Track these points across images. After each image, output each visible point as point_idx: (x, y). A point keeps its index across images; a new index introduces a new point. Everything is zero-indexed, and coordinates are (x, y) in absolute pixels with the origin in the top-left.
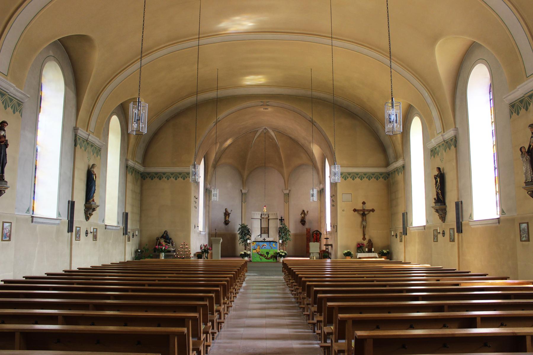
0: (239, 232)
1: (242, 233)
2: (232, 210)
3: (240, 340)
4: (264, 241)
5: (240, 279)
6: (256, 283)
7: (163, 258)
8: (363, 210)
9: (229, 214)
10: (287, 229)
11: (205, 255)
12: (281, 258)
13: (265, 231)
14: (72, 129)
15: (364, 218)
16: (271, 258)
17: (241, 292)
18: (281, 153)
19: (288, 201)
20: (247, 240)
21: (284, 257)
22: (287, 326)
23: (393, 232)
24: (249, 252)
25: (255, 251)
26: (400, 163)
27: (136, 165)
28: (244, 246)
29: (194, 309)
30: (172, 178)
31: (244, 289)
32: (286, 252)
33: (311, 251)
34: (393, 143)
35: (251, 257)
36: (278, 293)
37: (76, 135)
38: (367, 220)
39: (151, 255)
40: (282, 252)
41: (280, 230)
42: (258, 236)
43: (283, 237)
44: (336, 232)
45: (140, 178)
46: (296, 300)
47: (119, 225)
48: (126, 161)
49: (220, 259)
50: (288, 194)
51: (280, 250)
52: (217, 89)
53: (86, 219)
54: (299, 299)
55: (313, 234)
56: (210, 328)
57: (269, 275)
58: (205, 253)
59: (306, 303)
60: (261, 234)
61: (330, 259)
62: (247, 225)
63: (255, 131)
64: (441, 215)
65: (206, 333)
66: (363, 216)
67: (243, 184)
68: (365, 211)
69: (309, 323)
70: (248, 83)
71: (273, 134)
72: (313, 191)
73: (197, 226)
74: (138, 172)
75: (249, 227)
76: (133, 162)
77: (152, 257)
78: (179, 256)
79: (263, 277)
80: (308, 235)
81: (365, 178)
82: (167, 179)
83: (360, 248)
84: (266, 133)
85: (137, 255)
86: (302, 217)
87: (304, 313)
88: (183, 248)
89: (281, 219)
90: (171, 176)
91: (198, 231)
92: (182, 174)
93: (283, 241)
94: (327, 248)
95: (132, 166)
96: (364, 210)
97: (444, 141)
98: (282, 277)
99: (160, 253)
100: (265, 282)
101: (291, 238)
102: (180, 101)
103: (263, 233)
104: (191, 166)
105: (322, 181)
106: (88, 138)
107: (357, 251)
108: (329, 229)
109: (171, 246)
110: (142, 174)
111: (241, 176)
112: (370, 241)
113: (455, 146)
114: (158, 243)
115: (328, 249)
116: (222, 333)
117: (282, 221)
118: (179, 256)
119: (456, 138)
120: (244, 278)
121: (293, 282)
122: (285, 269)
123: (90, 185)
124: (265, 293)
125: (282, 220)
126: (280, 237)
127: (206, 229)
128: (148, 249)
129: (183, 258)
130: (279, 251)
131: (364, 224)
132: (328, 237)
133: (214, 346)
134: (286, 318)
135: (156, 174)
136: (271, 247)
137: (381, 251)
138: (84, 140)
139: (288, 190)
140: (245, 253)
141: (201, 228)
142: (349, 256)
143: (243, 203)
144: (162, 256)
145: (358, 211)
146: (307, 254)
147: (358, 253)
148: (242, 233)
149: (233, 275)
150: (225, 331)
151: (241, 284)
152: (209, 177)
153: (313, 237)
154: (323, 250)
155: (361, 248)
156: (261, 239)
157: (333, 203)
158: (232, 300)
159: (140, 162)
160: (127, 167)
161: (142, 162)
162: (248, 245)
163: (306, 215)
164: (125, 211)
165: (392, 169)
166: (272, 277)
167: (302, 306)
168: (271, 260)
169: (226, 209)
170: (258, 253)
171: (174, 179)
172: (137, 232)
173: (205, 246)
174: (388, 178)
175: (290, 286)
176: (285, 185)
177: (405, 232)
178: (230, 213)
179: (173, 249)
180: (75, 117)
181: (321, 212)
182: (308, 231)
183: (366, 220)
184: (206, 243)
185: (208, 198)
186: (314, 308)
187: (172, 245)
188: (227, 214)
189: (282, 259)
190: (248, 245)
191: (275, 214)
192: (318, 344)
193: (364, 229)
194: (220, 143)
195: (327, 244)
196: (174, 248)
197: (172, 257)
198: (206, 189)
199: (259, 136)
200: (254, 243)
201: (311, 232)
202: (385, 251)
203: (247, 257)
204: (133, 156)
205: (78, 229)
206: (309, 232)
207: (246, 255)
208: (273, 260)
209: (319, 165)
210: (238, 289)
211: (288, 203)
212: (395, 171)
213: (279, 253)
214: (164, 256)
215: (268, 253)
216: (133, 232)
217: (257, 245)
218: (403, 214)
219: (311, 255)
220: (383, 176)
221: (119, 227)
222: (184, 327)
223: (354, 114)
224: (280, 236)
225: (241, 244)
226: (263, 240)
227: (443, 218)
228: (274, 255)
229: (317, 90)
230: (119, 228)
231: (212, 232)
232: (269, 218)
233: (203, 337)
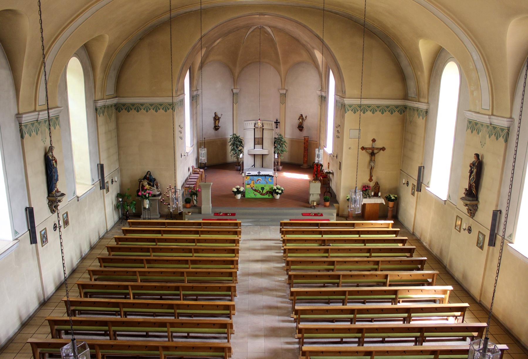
2: (222, 115)
8: (372, 149)
9: (219, 119)
12: (277, 195)
13: (259, 141)
14: (13, 117)
15: (373, 157)
16: (266, 194)
19: (285, 103)
23: (404, 180)
25: (249, 186)
30: (152, 110)
37: (20, 124)
38: (375, 160)
48: (95, 103)
50: (285, 95)
53: (52, 213)
64: (471, 210)
66: (372, 156)
71: (269, 30)
80: (306, 144)
82: (146, 111)
83: (365, 190)
89: (276, 121)
92: (163, 104)
96: (373, 149)
97: (491, 124)
106: (38, 118)
110: (116, 105)
111: (232, 72)
112: (377, 184)
113: (506, 141)
114: (141, 186)
117: (277, 125)
119: (509, 130)
123: (50, 174)
130: (275, 188)
131: (372, 165)
135: (133, 105)
143: (234, 104)
152: (195, 82)
160: (96, 110)
164: (100, 161)
168: (266, 196)
169: (215, 113)
170: (252, 188)
171: (154, 111)
172: (116, 178)
174: (405, 112)
178: (220, 118)
180: (16, 100)
183: (374, 161)
187: (157, 188)
188: (216, 119)
193: (372, 170)
200: (248, 177)
205: (43, 232)
208: (269, 196)
213: (275, 190)
214: (148, 203)
215: (263, 189)
216: (112, 178)
217: (251, 179)
218: (420, 168)
220: (398, 109)
224: (275, 147)
226: (258, 174)
227: (473, 210)
232: (263, 128)
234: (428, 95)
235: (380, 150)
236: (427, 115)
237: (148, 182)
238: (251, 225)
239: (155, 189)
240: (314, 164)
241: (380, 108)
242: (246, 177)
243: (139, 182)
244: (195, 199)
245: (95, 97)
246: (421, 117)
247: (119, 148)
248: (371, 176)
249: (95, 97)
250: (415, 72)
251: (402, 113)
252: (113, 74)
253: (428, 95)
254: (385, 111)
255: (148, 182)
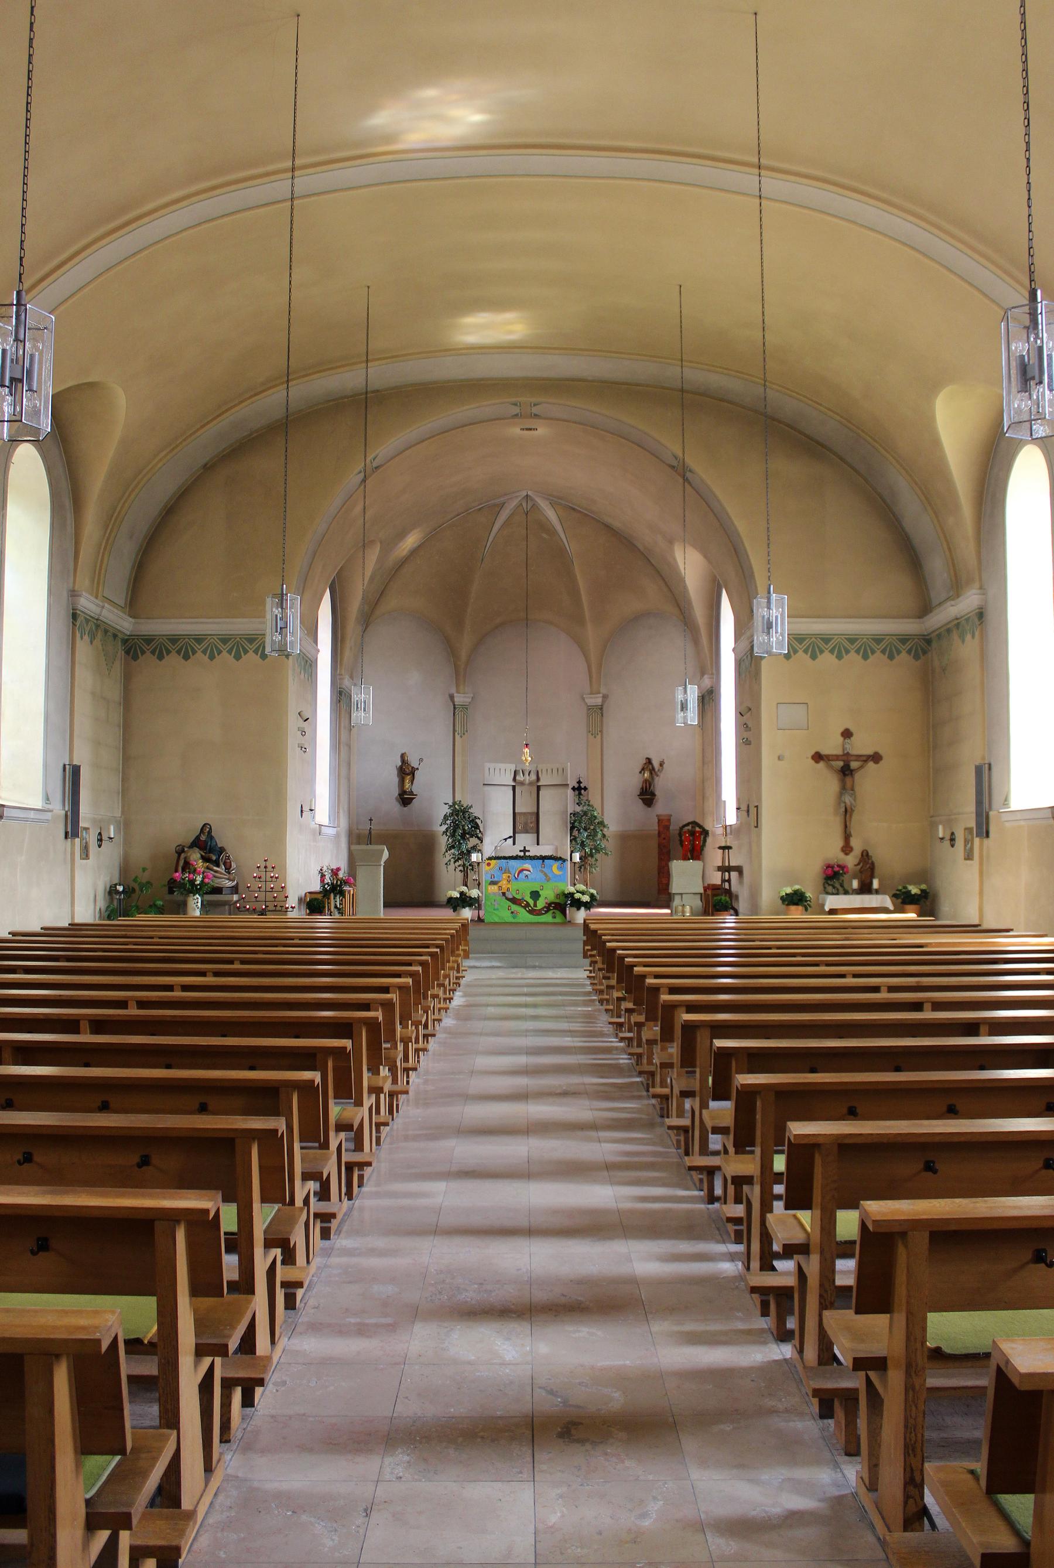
0: (444, 828)
1: (455, 831)
2: (421, 760)
3: (431, 1238)
4: (524, 856)
5: (443, 985)
6: (498, 995)
7: (197, 913)
9: (412, 772)
10: (595, 817)
11: (335, 901)
12: (579, 909)
15: (848, 779)
16: (546, 912)
17: (448, 1031)
18: (578, 578)
19: (601, 731)
20: (469, 853)
21: (588, 906)
22: (605, 1173)
23: (941, 828)
24: (474, 893)
25: (495, 888)
26: (968, 602)
27: (104, 610)
28: (460, 871)
29: (308, 1059)
30: (225, 653)
31: (458, 1017)
32: (594, 891)
33: (675, 887)
34: (945, 537)
35: (483, 908)
36: (570, 1031)
38: (857, 788)
39: (160, 903)
40: (583, 893)
41: (575, 821)
42: (506, 839)
43: (583, 845)
44: (757, 827)
45: (121, 653)
46: (632, 1061)
47: (50, 807)
48: (72, 596)
49: (382, 913)
50: (601, 709)
51: (575, 885)
52: (365, 359)
54: (645, 1061)
55: (680, 835)
56: (385, 1081)
57: (540, 967)
58: (332, 895)
59: (656, 1060)
60: (514, 832)
61: (737, 913)
62: (471, 806)
63: (495, 505)
65: (376, 1090)
66: (845, 775)
67: (457, 679)
68: (852, 758)
69: (691, 1168)
70: (471, 339)
71: (551, 514)
72: (685, 692)
73: (306, 810)
74: (115, 636)
75: (475, 811)
76: (97, 601)
77: (161, 911)
78: (248, 907)
79: (519, 973)
80: (663, 836)
81: (852, 654)
84: (529, 511)
85: (115, 903)
86: (646, 781)
87: (689, 1161)
88: (263, 879)
89: (576, 786)
90: (220, 646)
91: (314, 823)
93: (585, 857)
94: (727, 878)
95: (92, 615)
96: (846, 757)
98: (581, 974)
99: (187, 895)
100: (525, 990)
101: (609, 845)
102: (245, 400)
103: (521, 832)
104: (269, 600)
105: (710, 665)
107: (825, 888)
108: (731, 817)
109: (223, 872)
110: (127, 640)
112: (865, 856)
114: (181, 863)
115: (729, 881)
116: (368, 1203)
117: (580, 794)
118: (248, 907)
120: (458, 978)
121: (623, 999)
122: (591, 950)
124: (526, 1033)
125: (579, 789)
126: (574, 842)
127: (338, 817)
128: (148, 883)
129: (263, 913)
130: (572, 889)
131: (847, 801)
132: (728, 844)
133: (326, 1266)
134: (603, 1134)
135: (174, 639)
136: (545, 874)
137: (900, 888)
138: (88, 617)
139: (601, 695)
140: (462, 893)
141: (323, 813)
142: (797, 904)
143: (457, 737)
144: (195, 905)
145: (829, 760)
146: (662, 896)
147: (828, 893)
148: (455, 831)
149: (410, 980)
150: (377, 1195)
151: (445, 999)
152: (348, 654)
153: (681, 842)
154: (714, 885)
155: (838, 879)
156: (516, 851)
157: (746, 735)
158: (421, 1045)
159: (122, 603)
160: (74, 616)
161: (126, 600)
162: (472, 870)
163: (657, 776)
164: (71, 759)
165: (939, 625)
166: (550, 974)
167: (658, 1090)
168: (547, 918)
169: (403, 756)
170: (504, 894)
173: (335, 872)
175: (611, 1007)
176: (591, 681)
177: (983, 828)
178: (418, 769)
179: (230, 884)
181: (703, 763)
182: (664, 823)
183: (853, 790)
184: (342, 863)
185: (344, 722)
186: (653, 1031)
187: (228, 869)
188: (406, 771)
189: (581, 915)
190: (472, 870)
191: (560, 771)
192: (732, 1257)
193: (848, 816)
194: (381, 543)
195: (727, 864)
196: (233, 881)
197: (227, 907)
198: (340, 693)
199: (506, 524)
200: (493, 862)
201: (671, 828)
202: (914, 890)
203: (470, 906)
204: (95, 585)
206: (667, 827)
207: (464, 901)
208: (554, 917)
209: (699, 612)
210: (434, 1020)
211: (599, 737)
212: (949, 631)
213: (572, 895)
214: (199, 905)
215: (535, 895)
217: (500, 869)
218: (979, 770)
219: (677, 902)
220: (908, 646)
221: (51, 811)
222: (276, 1113)
223: (818, 442)
224: (573, 839)
225: (452, 866)
226: (522, 854)
228: (558, 901)
229: (698, 363)
230: (48, 816)
231: (360, 827)
232: (539, 784)
233: (303, 1189)
234: (980, 570)
235: (866, 761)
236: (982, 623)
237: (203, 854)
238: (498, 964)
239: (221, 873)
240: (682, 833)
241: (857, 644)
242: (487, 862)
243: (177, 855)
244: (336, 907)
245: (74, 582)
246: (968, 637)
247: (127, 759)
248: (847, 837)
249: (74, 582)
250: (938, 521)
251: (920, 658)
252: (127, 551)
253: (980, 570)
254: (873, 652)
255: (203, 854)
